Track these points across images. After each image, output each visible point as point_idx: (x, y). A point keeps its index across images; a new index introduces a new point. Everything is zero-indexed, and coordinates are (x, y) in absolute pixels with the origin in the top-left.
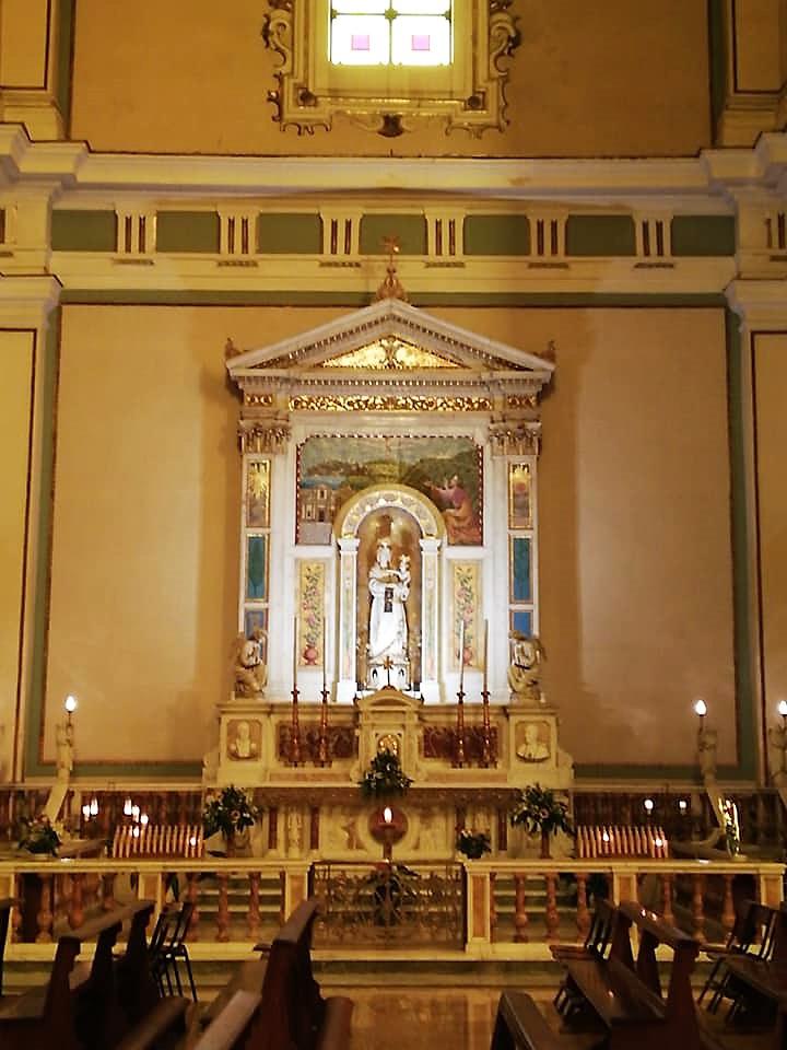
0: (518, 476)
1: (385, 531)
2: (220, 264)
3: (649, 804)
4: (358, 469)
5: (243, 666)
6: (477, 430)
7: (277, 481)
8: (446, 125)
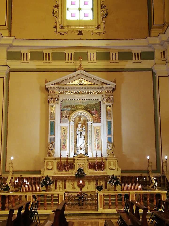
0: (108, 108)
1: (80, 120)
3: (137, 179)
5: (50, 150)
7: (56, 109)
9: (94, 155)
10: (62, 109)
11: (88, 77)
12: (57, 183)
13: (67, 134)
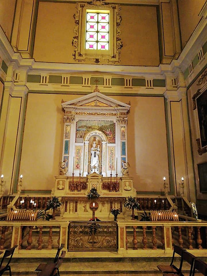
0: (123, 129)
1: (95, 140)
2: (61, 86)
3: (155, 201)
4: (89, 127)
5: (62, 168)
6: (114, 119)
7: (72, 129)
8: (108, 61)
9: (107, 175)
10: (77, 129)
11: (103, 99)
12: (68, 204)
13: (82, 154)
